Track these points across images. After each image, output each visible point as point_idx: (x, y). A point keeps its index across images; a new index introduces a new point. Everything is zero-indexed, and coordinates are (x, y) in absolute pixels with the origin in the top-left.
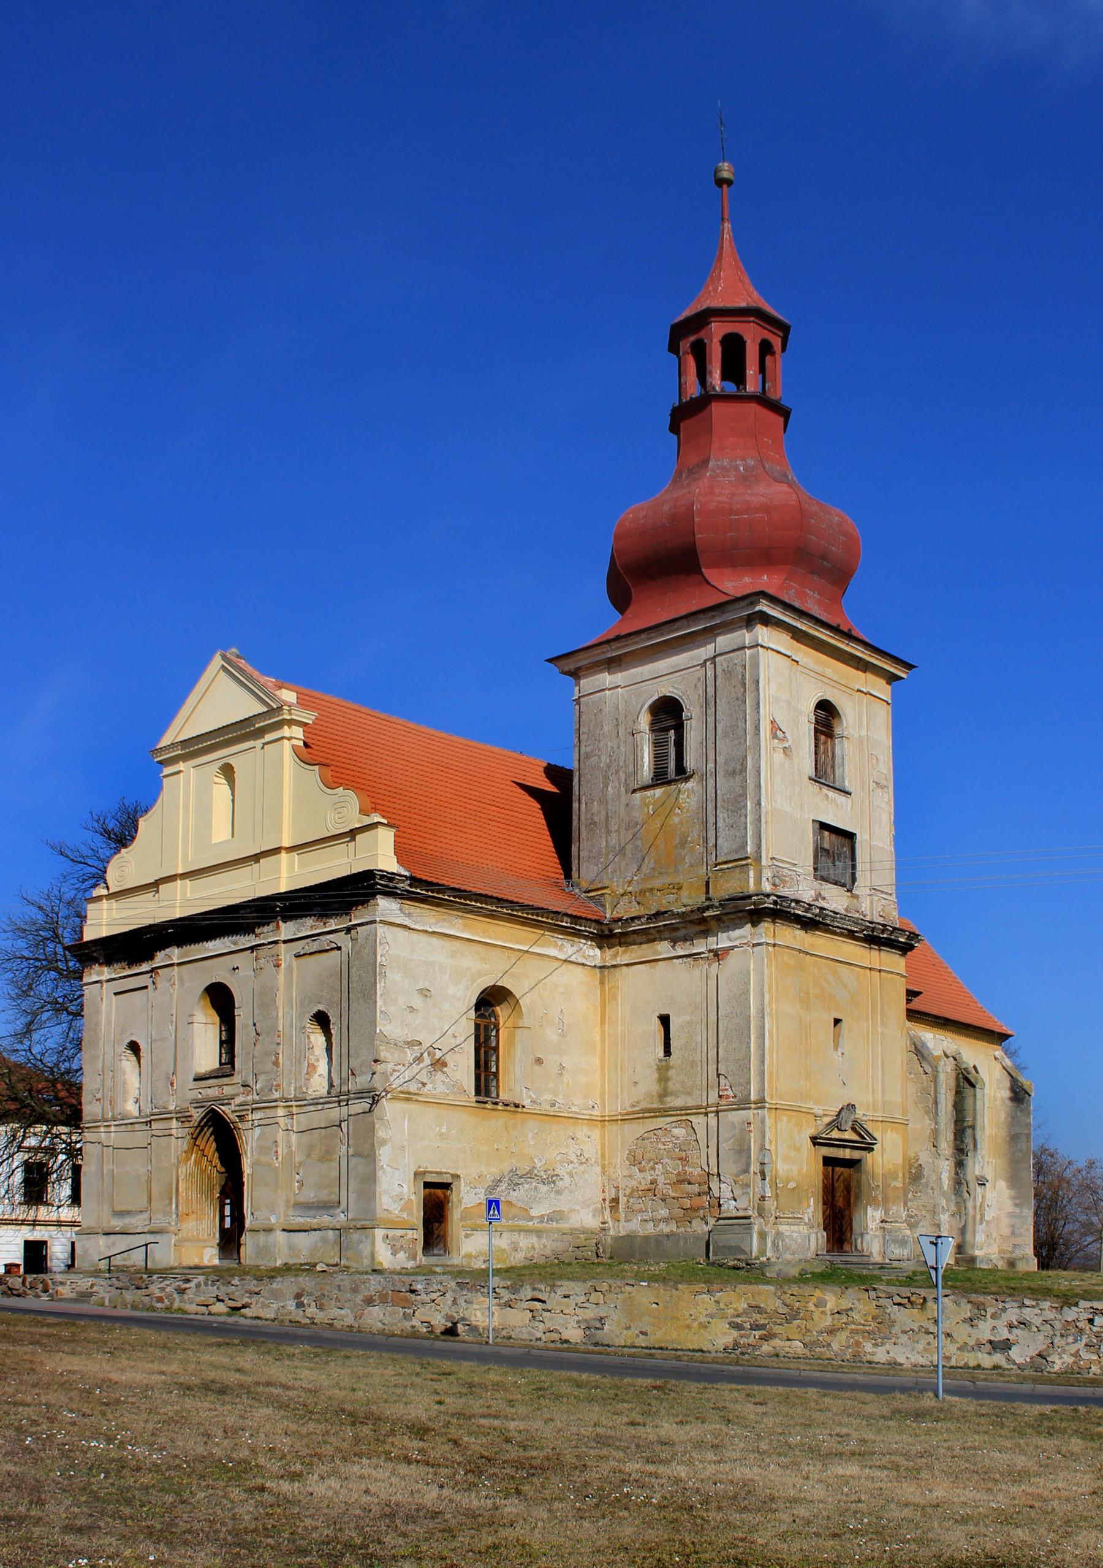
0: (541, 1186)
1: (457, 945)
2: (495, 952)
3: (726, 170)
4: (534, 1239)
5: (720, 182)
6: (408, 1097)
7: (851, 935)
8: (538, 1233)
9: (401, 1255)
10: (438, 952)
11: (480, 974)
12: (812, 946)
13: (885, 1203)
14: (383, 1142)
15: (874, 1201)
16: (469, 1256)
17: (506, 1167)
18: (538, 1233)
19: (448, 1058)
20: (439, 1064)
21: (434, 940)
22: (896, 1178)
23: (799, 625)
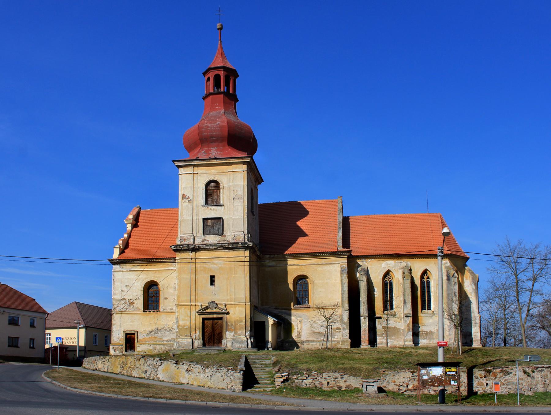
0: (167, 332)
1: (138, 272)
2: (150, 272)
3: (219, 26)
4: (162, 346)
5: (221, 29)
6: (121, 312)
7: (216, 249)
8: (163, 345)
9: (117, 352)
10: (132, 276)
11: (146, 279)
12: (200, 256)
13: (235, 330)
14: (114, 324)
15: (231, 331)
16: (139, 351)
17: (154, 327)
18: (163, 345)
19: (134, 302)
20: (132, 303)
21: (131, 273)
22: (242, 321)
23: (193, 163)
